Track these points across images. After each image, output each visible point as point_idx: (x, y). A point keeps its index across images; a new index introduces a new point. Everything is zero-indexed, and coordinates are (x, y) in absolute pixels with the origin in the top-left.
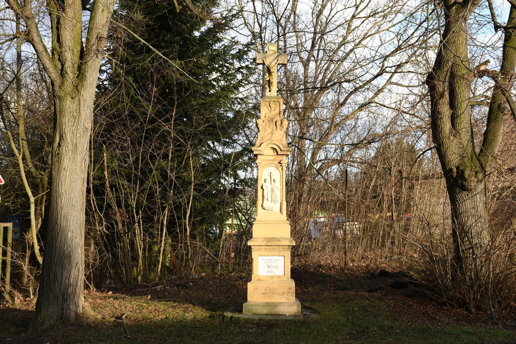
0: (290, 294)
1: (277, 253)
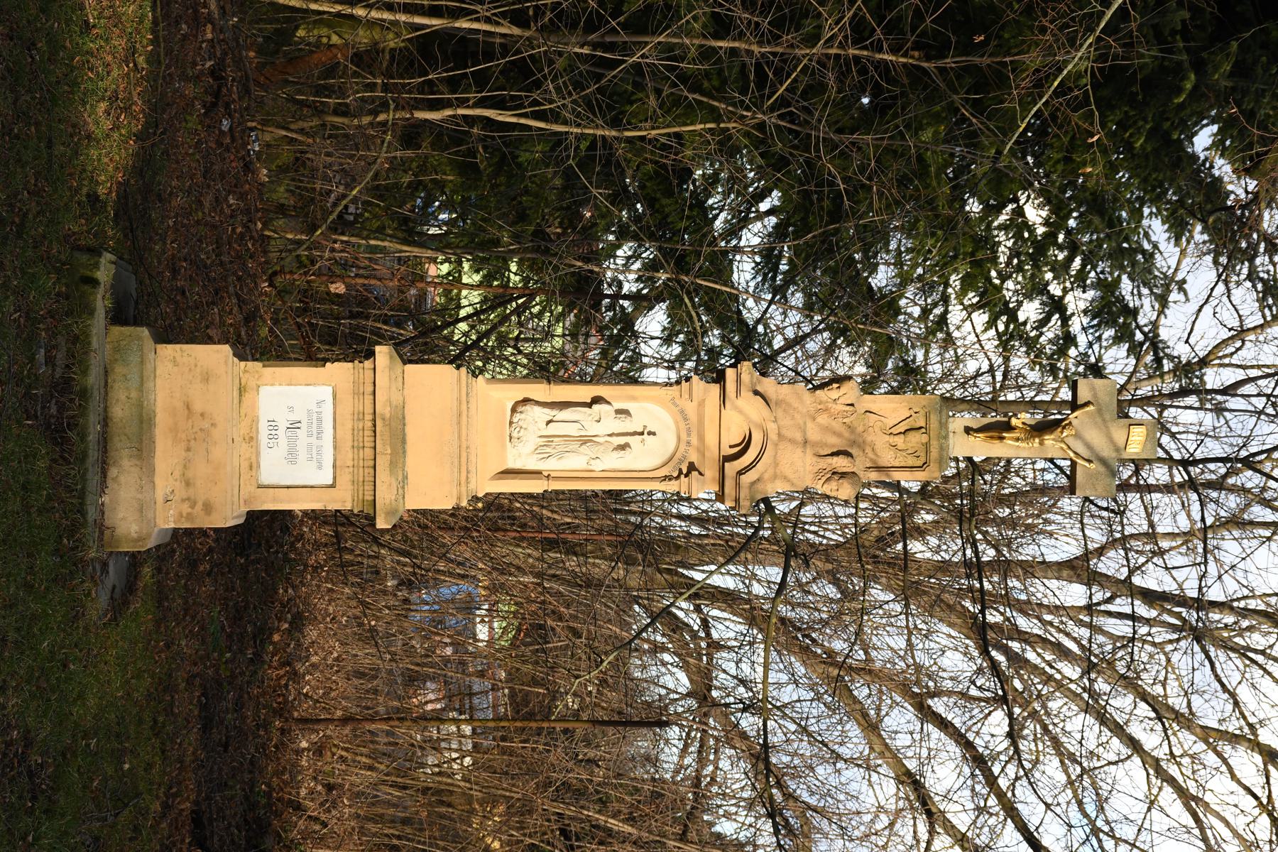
0: (185, 508)
1: (348, 456)
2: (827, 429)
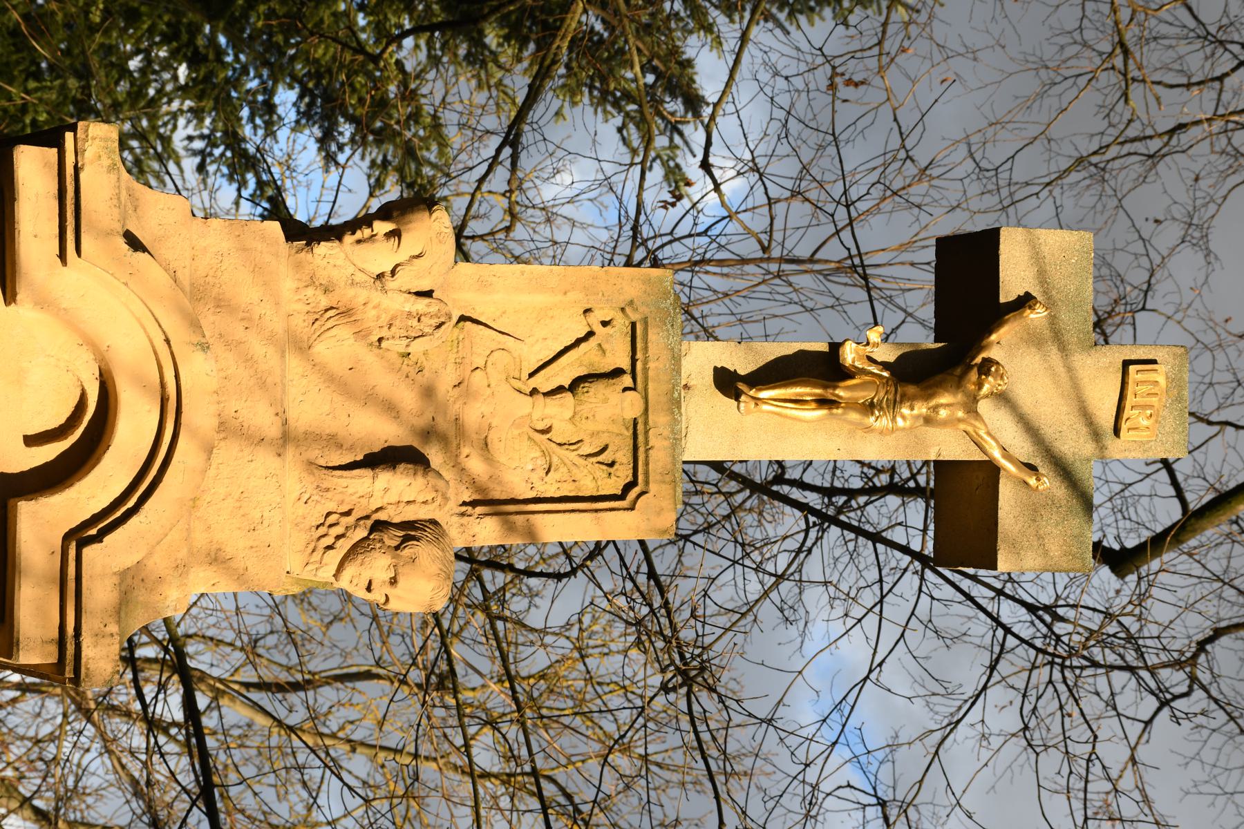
2: (344, 385)
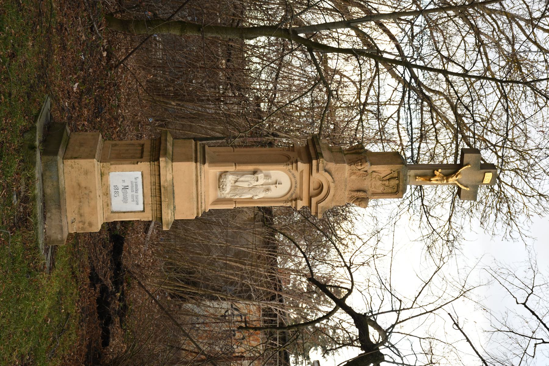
0: (81, 225)
1: (149, 200)
